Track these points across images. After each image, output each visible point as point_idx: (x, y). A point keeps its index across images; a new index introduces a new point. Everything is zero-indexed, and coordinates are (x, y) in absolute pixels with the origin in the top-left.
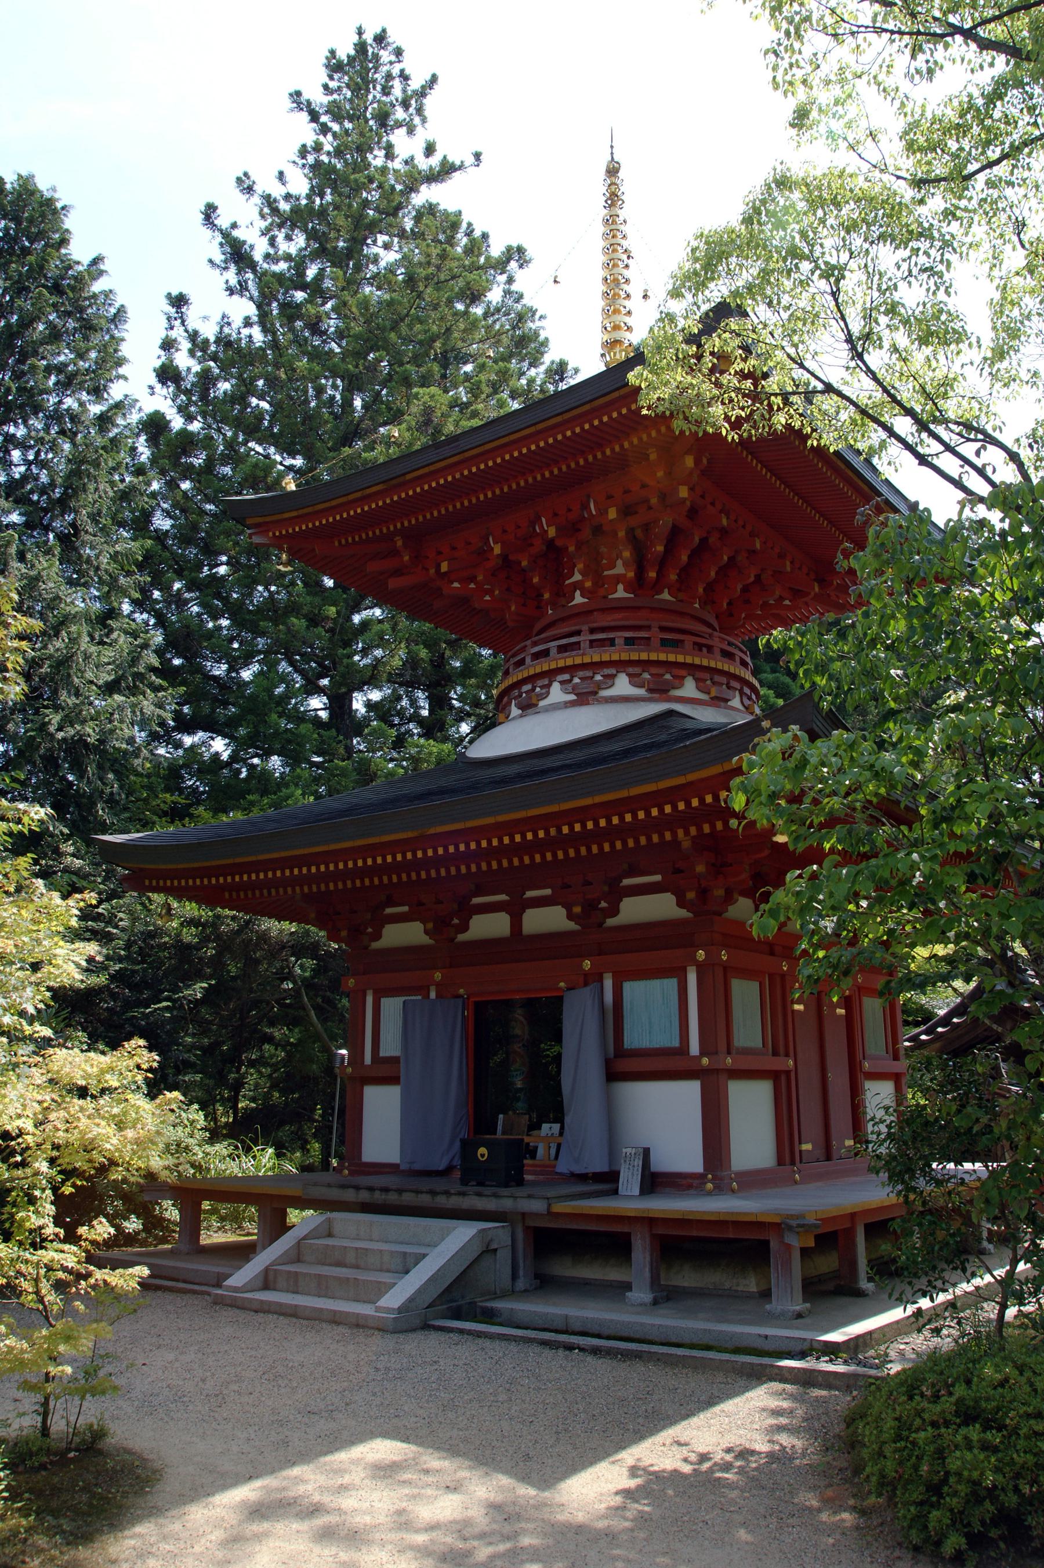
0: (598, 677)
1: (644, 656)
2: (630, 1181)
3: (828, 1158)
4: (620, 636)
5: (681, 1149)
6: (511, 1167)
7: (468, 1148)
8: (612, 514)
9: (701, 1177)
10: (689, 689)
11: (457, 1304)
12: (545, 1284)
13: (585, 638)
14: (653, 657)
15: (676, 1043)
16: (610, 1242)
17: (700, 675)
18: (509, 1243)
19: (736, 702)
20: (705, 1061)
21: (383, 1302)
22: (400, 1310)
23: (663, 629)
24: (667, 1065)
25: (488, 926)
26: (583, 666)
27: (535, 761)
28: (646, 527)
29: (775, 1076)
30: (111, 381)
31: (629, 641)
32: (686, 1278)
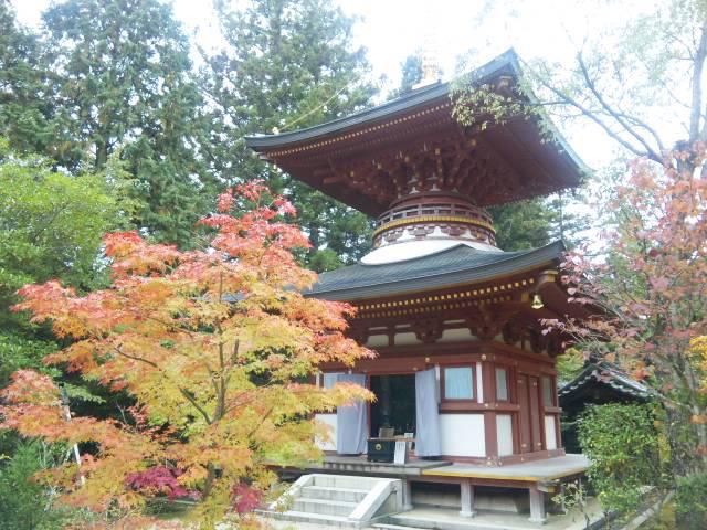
0: (426, 228)
1: (448, 219)
3: (532, 451)
4: (436, 209)
7: (371, 444)
8: (438, 152)
9: (486, 458)
12: (416, 506)
13: (420, 209)
14: (453, 219)
15: (472, 397)
17: (473, 227)
19: (487, 241)
20: (486, 405)
21: (351, 516)
22: (360, 520)
23: (457, 206)
24: (467, 408)
26: (419, 223)
27: (401, 266)
28: (450, 159)
29: (513, 413)
30: (297, 26)
31: (440, 211)
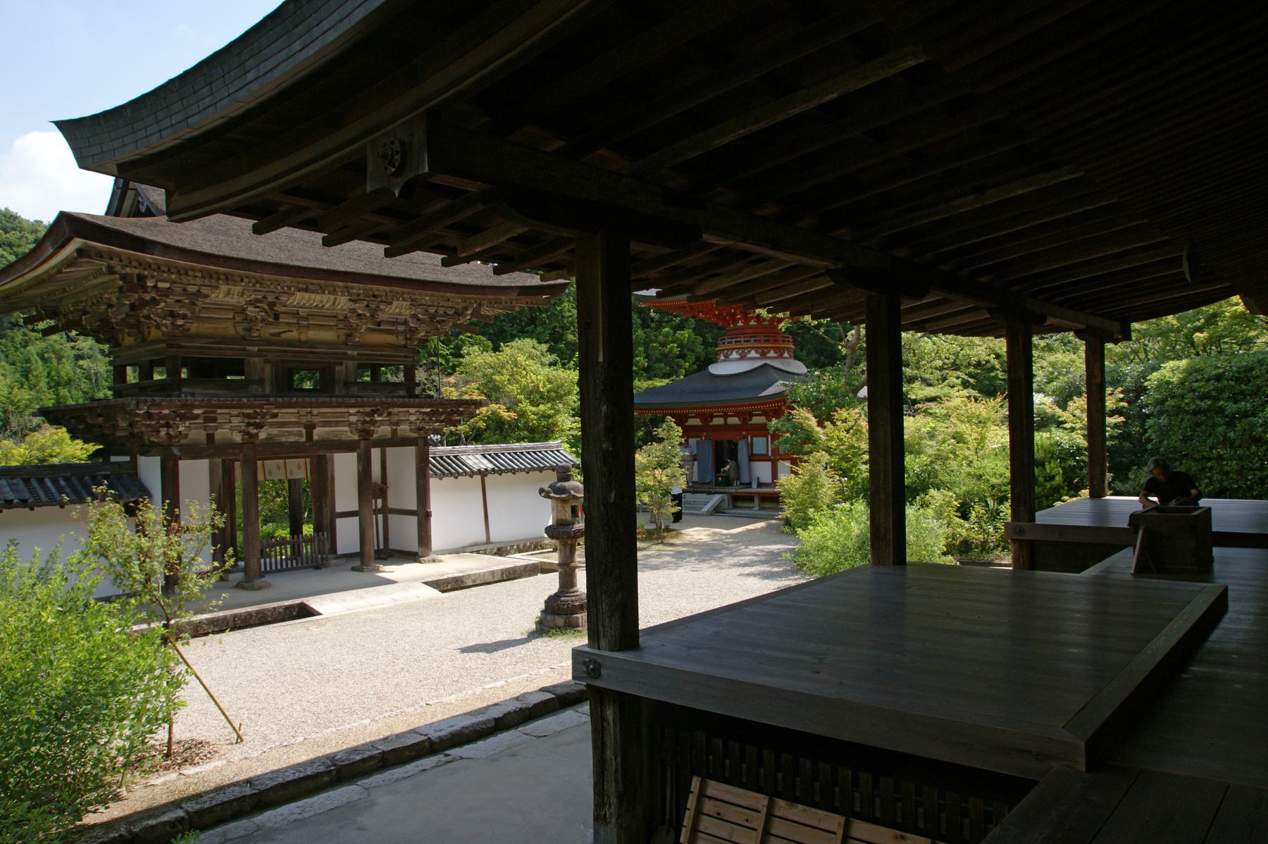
2: (754, 485)
5: (766, 478)
6: (728, 482)
7: (716, 478)
10: (772, 354)
11: (717, 511)
12: (735, 507)
16: (750, 498)
18: (433, 482)
24: (763, 458)
25: (718, 421)
32: (767, 505)
